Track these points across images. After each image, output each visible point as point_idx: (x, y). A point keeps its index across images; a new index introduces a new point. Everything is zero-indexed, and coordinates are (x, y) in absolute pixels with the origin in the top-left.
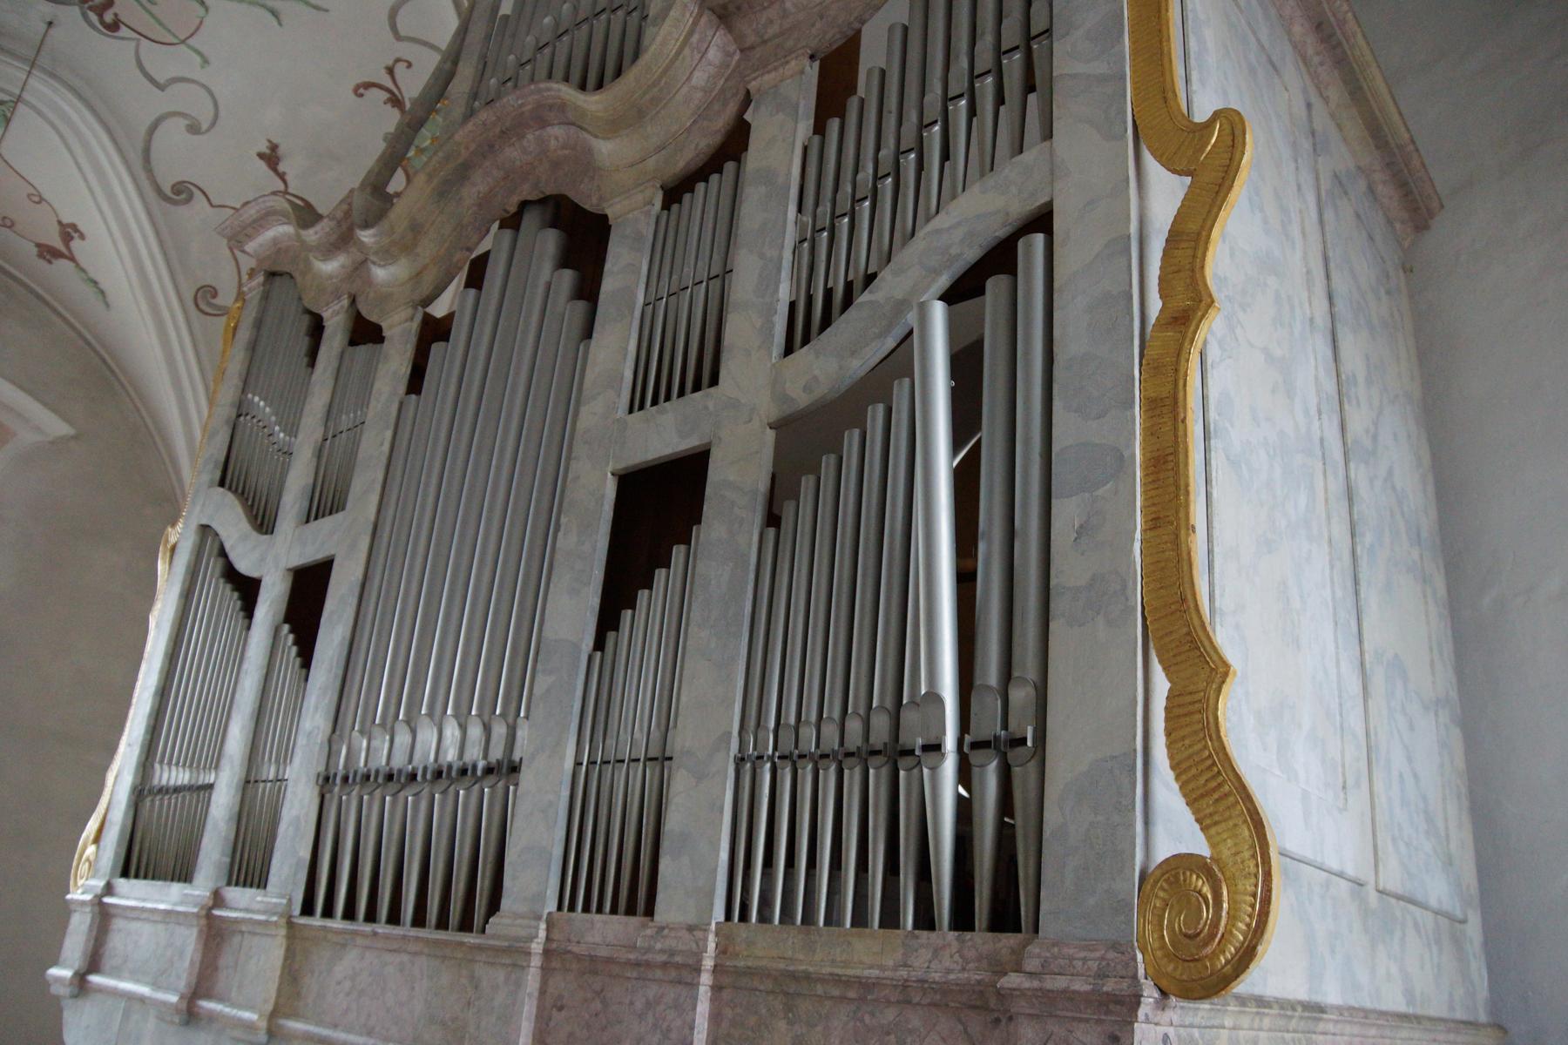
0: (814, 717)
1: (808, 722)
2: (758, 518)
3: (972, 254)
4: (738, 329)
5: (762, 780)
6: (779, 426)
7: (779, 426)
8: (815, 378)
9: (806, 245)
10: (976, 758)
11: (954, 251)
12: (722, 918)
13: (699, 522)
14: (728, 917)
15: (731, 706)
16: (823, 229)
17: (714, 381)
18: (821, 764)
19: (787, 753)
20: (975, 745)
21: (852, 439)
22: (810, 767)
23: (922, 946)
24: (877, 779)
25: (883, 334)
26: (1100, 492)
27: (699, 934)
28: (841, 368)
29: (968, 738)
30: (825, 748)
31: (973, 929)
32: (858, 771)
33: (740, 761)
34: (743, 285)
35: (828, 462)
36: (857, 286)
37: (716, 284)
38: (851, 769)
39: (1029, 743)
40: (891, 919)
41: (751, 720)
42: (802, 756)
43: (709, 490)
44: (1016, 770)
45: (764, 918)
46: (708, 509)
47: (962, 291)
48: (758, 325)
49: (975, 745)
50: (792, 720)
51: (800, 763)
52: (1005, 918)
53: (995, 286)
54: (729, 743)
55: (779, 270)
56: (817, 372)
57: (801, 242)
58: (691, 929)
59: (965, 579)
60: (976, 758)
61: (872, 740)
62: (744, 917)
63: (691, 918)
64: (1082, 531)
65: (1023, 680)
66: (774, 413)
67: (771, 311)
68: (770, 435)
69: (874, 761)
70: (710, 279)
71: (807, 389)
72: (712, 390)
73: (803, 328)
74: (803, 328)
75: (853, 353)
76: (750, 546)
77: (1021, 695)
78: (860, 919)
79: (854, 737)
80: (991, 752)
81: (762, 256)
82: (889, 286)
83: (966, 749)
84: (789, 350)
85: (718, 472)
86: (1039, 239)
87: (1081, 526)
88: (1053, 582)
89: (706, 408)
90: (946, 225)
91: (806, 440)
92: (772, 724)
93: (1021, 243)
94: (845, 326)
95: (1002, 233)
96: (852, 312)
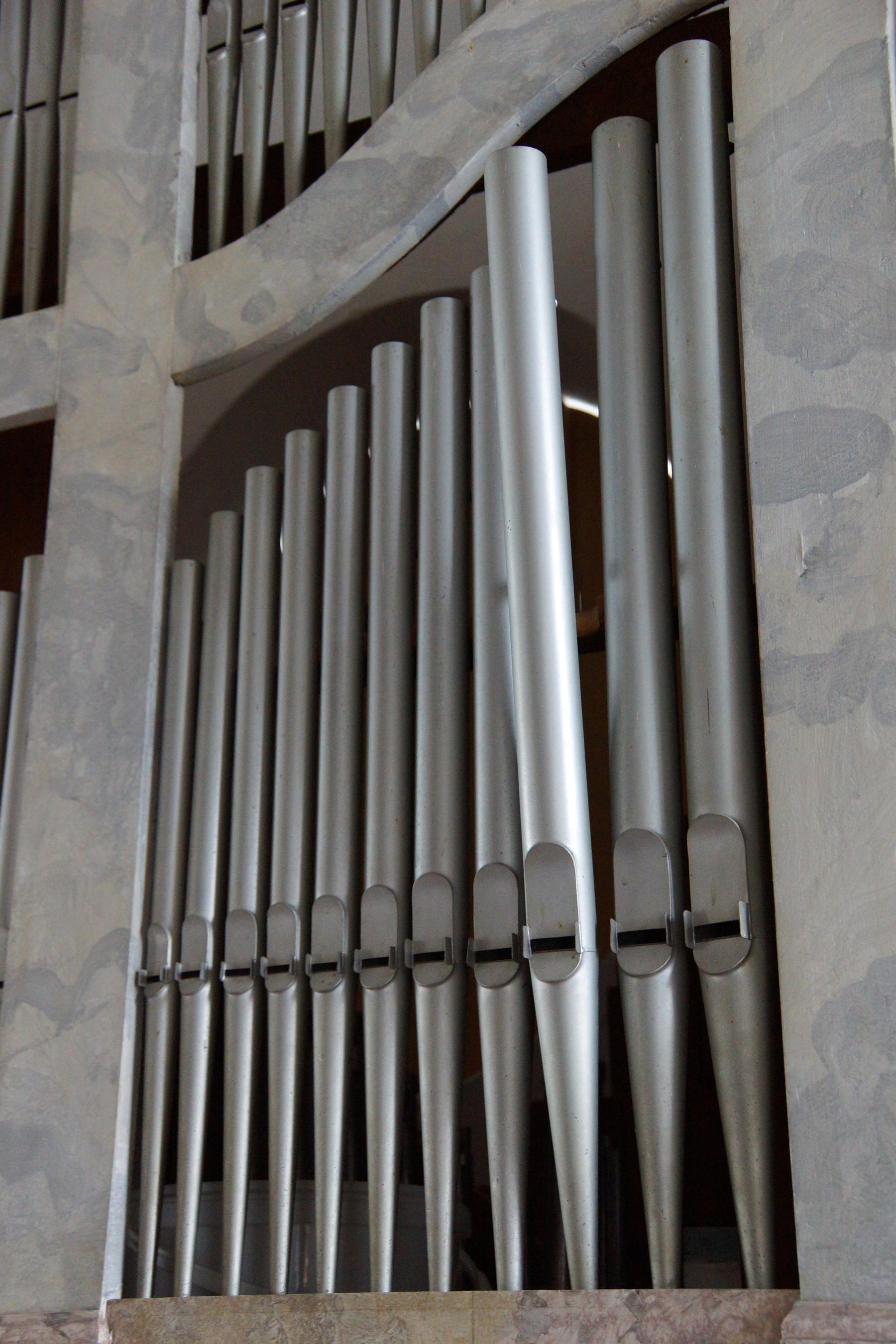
0: (295, 898)
1: (284, 906)
2: (160, 543)
3: (566, 79)
4: (91, 204)
5: (194, 1018)
6: (186, 381)
7: (186, 381)
8: (266, 296)
9: (224, 55)
10: (631, 960)
11: (532, 71)
12: (117, 1294)
13: (38, 547)
14: (130, 1287)
15: (126, 881)
16: (258, 28)
17: (50, 295)
18: (317, 981)
19: (244, 963)
20: (630, 939)
21: (343, 402)
22: (293, 989)
23: (555, 1321)
24: (434, 1005)
25: (401, 219)
26: (846, 492)
27: (73, 1329)
28: (316, 277)
29: (616, 927)
30: (322, 951)
31: (648, 1285)
32: (390, 995)
33: (148, 982)
34: (104, 116)
35: (298, 444)
36: (332, 143)
37: (39, 122)
38: (378, 988)
39: (744, 933)
40: (476, 1265)
41: (168, 899)
42: (274, 969)
43: (56, 492)
44: (713, 984)
45: (210, 1282)
46: (56, 526)
47: (562, 136)
48: (141, 195)
49: (630, 939)
50: (252, 903)
51: (272, 982)
52: (709, 1253)
53: (614, 138)
54: (126, 950)
55: (178, 101)
56: (268, 284)
57: (214, 49)
58: (55, 1321)
59: (591, 645)
60: (631, 960)
61: (417, 934)
62: (165, 1284)
63: (54, 1298)
64: (816, 558)
65: (718, 822)
66: (185, 358)
67: (167, 170)
68: (176, 396)
69: (424, 973)
70: (25, 108)
71: (248, 313)
72: (50, 313)
73: (230, 206)
74: (230, 206)
75: (341, 252)
76: (149, 592)
77: (717, 856)
78: (411, 1273)
79: (381, 929)
80: (663, 950)
81: (138, 69)
82: (400, 136)
83: (613, 946)
84: (200, 247)
85: (71, 462)
86: (700, 51)
87: (814, 551)
88: (765, 650)
89: (42, 344)
90: (515, 24)
91: (254, 415)
92: (210, 912)
93: (665, 62)
94: (310, 211)
95: (624, 39)
96: (437, 71)
